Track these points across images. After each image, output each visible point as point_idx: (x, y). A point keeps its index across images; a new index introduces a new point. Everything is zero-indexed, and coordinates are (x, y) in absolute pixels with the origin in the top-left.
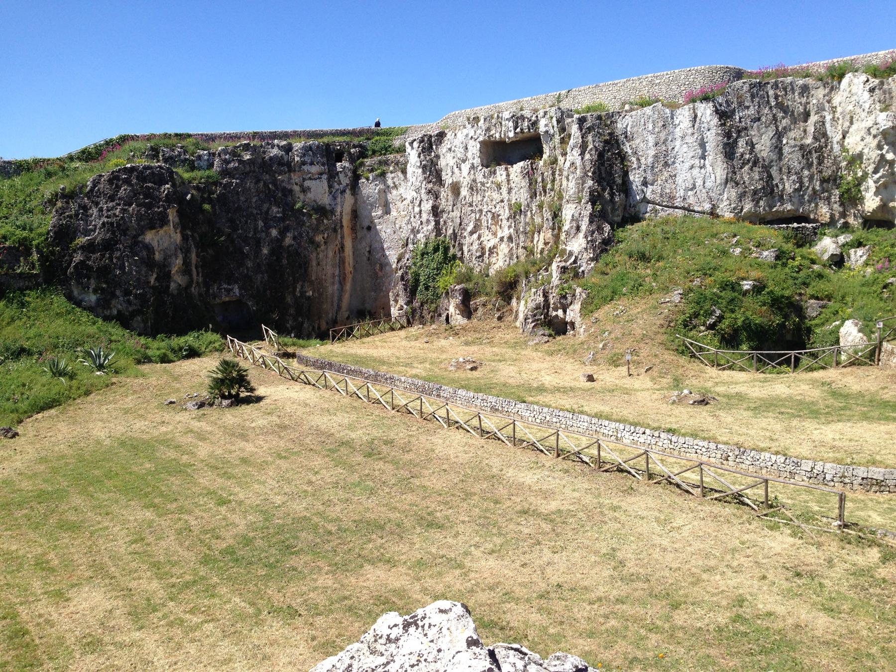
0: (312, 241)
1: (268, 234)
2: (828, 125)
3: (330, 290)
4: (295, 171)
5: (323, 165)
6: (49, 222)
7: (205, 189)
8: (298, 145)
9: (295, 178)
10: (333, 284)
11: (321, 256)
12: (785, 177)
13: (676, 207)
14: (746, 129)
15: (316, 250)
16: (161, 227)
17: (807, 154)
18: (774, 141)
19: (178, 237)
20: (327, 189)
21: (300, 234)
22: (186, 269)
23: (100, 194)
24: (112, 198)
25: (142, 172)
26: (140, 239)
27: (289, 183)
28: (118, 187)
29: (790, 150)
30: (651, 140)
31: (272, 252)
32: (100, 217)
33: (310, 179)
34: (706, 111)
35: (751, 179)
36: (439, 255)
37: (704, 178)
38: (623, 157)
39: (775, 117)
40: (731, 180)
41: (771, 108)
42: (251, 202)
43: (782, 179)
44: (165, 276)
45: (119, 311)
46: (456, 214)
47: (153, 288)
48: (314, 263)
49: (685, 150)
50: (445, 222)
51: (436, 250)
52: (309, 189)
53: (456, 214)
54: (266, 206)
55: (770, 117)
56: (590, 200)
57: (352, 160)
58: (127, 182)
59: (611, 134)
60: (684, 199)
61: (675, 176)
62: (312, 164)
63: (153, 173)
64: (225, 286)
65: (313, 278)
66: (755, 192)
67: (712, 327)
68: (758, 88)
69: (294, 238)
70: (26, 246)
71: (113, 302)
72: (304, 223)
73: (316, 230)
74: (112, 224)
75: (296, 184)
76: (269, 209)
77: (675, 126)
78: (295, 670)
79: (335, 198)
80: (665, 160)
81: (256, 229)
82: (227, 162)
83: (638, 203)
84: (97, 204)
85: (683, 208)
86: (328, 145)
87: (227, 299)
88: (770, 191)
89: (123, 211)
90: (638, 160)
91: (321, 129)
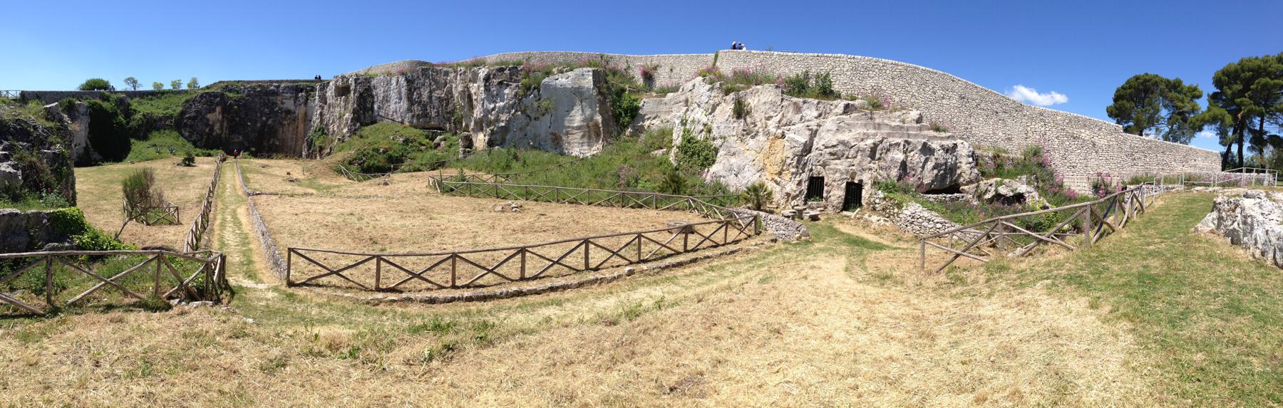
0: (281, 123)
2: (453, 90)
3: (290, 143)
5: (293, 93)
6: (179, 109)
7: (237, 101)
8: (283, 85)
9: (279, 98)
10: (292, 141)
14: (419, 88)
21: (276, 121)
22: (221, 128)
30: (382, 89)
34: (402, 80)
36: (320, 133)
38: (373, 97)
39: (430, 84)
40: (409, 110)
44: (212, 130)
48: (281, 132)
51: (319, 130)
54: (262, 108)
57: (307, 92)
58: (205, 97)
66: (418, 115)
67: (360, 164)
68: (425, 72)
69: (273, 121)
72: (278, 116)
73: (285, 119)
80: (386, 99)
82: (249, 91)
86: (297, 86)
88: (425, 115)
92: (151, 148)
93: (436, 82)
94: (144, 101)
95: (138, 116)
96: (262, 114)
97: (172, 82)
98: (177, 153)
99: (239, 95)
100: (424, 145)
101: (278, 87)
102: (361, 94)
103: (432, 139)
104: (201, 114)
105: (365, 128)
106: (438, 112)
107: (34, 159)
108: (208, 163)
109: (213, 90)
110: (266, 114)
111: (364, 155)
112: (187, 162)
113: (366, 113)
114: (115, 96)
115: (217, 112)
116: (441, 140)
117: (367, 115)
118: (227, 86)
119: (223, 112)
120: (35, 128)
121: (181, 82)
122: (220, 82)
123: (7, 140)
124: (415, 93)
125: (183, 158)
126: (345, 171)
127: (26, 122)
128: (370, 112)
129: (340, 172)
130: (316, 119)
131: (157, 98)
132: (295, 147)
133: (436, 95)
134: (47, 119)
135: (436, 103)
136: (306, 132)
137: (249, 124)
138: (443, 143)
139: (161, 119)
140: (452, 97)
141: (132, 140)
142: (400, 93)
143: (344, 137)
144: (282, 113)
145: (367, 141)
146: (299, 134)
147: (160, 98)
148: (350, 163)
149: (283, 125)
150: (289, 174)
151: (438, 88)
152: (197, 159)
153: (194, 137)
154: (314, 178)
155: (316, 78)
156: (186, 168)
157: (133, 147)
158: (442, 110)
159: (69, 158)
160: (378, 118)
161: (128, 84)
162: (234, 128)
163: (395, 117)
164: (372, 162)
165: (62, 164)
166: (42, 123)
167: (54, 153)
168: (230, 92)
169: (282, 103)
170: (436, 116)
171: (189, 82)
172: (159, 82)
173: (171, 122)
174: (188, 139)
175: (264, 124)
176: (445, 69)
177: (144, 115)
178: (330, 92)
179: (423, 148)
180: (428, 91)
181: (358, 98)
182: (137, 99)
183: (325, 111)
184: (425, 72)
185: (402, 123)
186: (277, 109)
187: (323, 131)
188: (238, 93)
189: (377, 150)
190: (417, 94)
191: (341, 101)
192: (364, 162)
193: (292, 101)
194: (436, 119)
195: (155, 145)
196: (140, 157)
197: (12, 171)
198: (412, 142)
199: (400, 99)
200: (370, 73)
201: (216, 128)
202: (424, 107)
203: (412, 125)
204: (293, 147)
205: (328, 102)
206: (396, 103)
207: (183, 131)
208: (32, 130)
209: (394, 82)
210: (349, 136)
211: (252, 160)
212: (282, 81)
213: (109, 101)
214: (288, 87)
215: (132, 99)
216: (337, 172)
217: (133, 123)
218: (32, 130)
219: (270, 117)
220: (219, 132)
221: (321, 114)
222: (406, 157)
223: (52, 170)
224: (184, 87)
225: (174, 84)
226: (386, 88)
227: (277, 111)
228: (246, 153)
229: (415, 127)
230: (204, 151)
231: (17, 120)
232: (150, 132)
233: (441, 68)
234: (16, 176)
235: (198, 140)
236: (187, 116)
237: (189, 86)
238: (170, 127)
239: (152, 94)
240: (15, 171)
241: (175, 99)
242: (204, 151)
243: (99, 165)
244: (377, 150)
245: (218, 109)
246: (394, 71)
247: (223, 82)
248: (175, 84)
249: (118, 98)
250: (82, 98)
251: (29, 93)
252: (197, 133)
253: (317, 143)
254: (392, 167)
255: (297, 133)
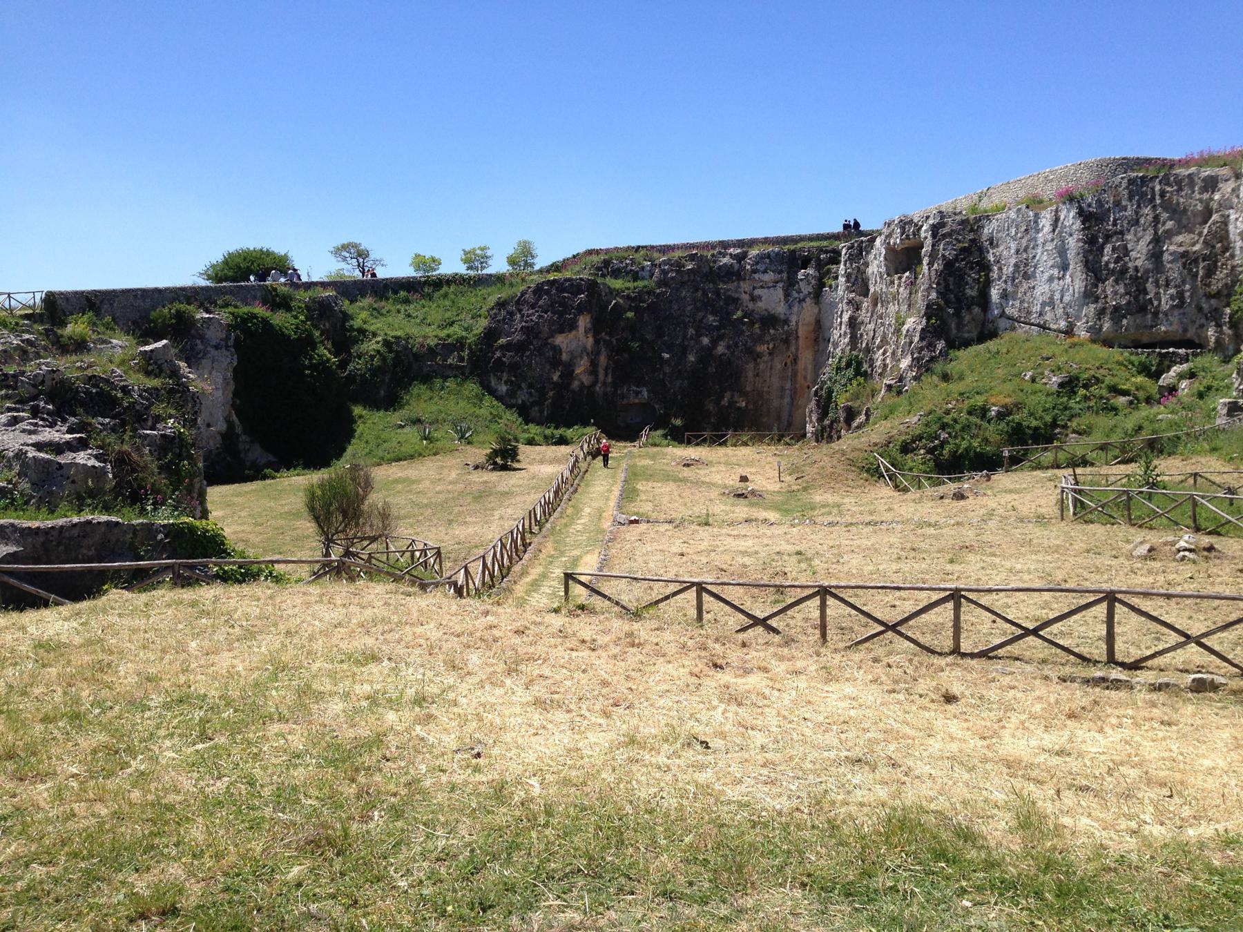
1: (698, 342)
3: (775, 403)
4: (744, 279)
5: (780, 272)
6: (483, 323)
7: (634, 300)
8: (754, 252)
9: (745, 286)
11: (762, 367)
12: (1162, 291)
13: (1032, 324)
14: (1122, 233)
15: (755, 360)
16: (570, 331)
17: (1190, 264)
18: (1151, 247)
19: (590, 342)
20: (783, 298)
21: (736, 344)
23: (526, 302)
24: (533, 307)
25: (563, 284)
26: (550, 341)
27: (736, 292)
28: (540, 298)
29: (1170, 258)
30: (1013, 246)
31: (700, 360)
32: (521, 321)
33: (762, 287)
34: (1069, 217)
35: (1115, 293)
37: (1062, 291)
38: (985, 267)
40: (1089, 295)
41: (1154, 207)
42: (684, 311)
43: (1157, 294)
44: (568, 373)
45: (523, 401)
46: (871, 326)
47: (555, 384)
48: (750, 374)
49: (1045, 258)
50: (862, 335)
51: (848, 365)
52: (760, 297)
53: (871, 326)
54: (701, 314)
55: (1150, 218)
56: (926, 314)
57: (820, 265)
58: (548, 292)
59: (973, 241)
60: (1041, 314)
61: (1034, 288)
62: (765, 272)
63: (572, 285)
64: (634, 388)
65: (748, 389)
66: (1117, 309)
67: (930, 451)
68: (1139, 189)
69: (728, 347)
70: (461, 343)
71: (519, 393)
72: (743, 332)
73: (760, 340)
74: (528, 327)
75: (745, 293)
76: (704, 317)
77: (1038, 231)
78: (980, 931)
79: (790, 307)
80: (1024, 271)
81: (685, 336)
82: (664, 272)
83: (996, 318)
84: (520, 311)
85: (1038, 325)
87: (637, 401)
88: (1140, 306)
89: (540, 317)
90: (1000, 269)
91: (798, 234)
92: (407, 430)
93: (1176, 212)
94: (387, 305)
95: (371, 346)
96: (701, 328)
97: (466, 253)
98: (475, 439)
99: (640, 284)
100: (1125, 393)
101: (741, 258)
102: (948, 264)
103: (1156, 376)
104: (537, 337)
105: (962, 354)
106: (1181, 295)
107: (126, 447)
108: (556, 461)
109: (568, 274)
110: (710, 329)
111: (944, 427)
112: (499, 460)
113: (964, 313)
114: (303, 296)
115: (581, 330)
116: (1181, 376)
117: (967, 318)
118: (607, 263)
119: (596, 328)
120: (125, 390)
121: (489, 253)
122: (589, 252)
123: (74, 415)
124: (1108, 249)
125: (489, 451)
126: (887, 470)
127: (107, 381)
128: (976, 310)
129: (875, 473)
130: (839, 336)
131: (423, 297)
132: (790, 415)
133: (1172, 248)
134: (148, 374)
135: (1174, 271)
136: (818, 365)
137: (666, 356)
138: (1184, 384)
139: (432, 351)
140: (1226, 249)
141: (357, 410)
142: (1062, 251)
143: (901, 379)
144: (752, 323)
145: (956, 387)
146: (799, 378)
147: (430, 297)
148: (906, 449)
149: (756, 356)
150: (744, 479)
151: (1184, 227)
152: (524, 451)
153: (522, 397)
154: (805, 489)
155: (846, 227)
156: (495, 476)
157: (360, 428)
158: (1194, 289)
159: (193, 445)
160: (1003, 323)
161: (345, 259)
162: (626, 370)
163: (1048, 316)
164: (964, 444)
165: (180, 457)
166: (138, 382)
167: (164, 436)
168: (616, 278)
169: (754, 299)
170: (1173, 307)
171: (512, 251)
172: (428, 254)
173: (461, 359)
174: (506, 401)
175: (706, 355)
176: (1207, 172)
177: (386, 343)
178: (876, 265)
179: (1123, 400)
180: (1148, 238)
181: (940, 274)
182: (367, 301)
183: (864, 315)
184: (1139, 189)
185: (1069, 332)
186: (739, 313)
187: (858, 367)
188: (636, 277)
189: (983, 412)
190: (1114, 249)
191: (899, 286)
192: (943, 444)
193: (779, 293)
194: (1175, 319)
195: (417, 421)
196: (380, 453)
197: (97, 464)
198: (1086, 386)
199: (1064, 267)
200: (985, 205)
201: (578, 371)
202: (1138, 284)
203: (1098, 337)
204: (785, 415)
205: (872, 290)
206: (1051, 279)
207: (493, 382)
208: (120, 395)
209: (1046, 222)
210: (915, 378)
211: (670, 450)
212: (752, 243)
213: (288, 309)
214: (768, 256)
215: (352, 302)
216: (868, 471)
217: (356, 366)
218: (120, 395)
219: (721, 338)
220: (586, 380)
221: (853, 324)
222: (1065, 427)
223: (160, 468)
224: (498, 265)
225: (471, 259)
226: (1024, 242)
227: (740, 320)
228: (660, 432)
229: (1108, 343)
230: (548, 432)
231: (90, 378)
232: (406, 387)
233: (1193, 170)
234: (103, 470)
235: (533, 404)
236: (502, 341)
237: (512, 262)
238: (463, 374)
239: (408, 285)
240: (102, 465)
241: (471, 299)
242: (548, 432)
243: (264, 478)
244: (983, 412)
245: (583, 322)
246: (1048, 193)
247: (598, 252)
248: (474, 258)
249: (313, 300)
250: (214, 303)
251: (66, 296)
252: (530, 386)
253: (842, 400)
254: (1006, 454)
255: (795, 374)
